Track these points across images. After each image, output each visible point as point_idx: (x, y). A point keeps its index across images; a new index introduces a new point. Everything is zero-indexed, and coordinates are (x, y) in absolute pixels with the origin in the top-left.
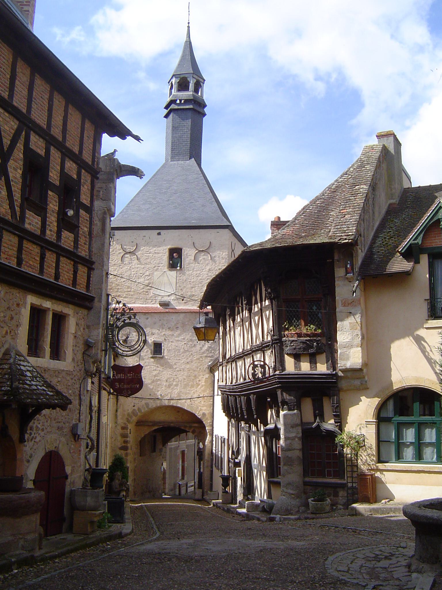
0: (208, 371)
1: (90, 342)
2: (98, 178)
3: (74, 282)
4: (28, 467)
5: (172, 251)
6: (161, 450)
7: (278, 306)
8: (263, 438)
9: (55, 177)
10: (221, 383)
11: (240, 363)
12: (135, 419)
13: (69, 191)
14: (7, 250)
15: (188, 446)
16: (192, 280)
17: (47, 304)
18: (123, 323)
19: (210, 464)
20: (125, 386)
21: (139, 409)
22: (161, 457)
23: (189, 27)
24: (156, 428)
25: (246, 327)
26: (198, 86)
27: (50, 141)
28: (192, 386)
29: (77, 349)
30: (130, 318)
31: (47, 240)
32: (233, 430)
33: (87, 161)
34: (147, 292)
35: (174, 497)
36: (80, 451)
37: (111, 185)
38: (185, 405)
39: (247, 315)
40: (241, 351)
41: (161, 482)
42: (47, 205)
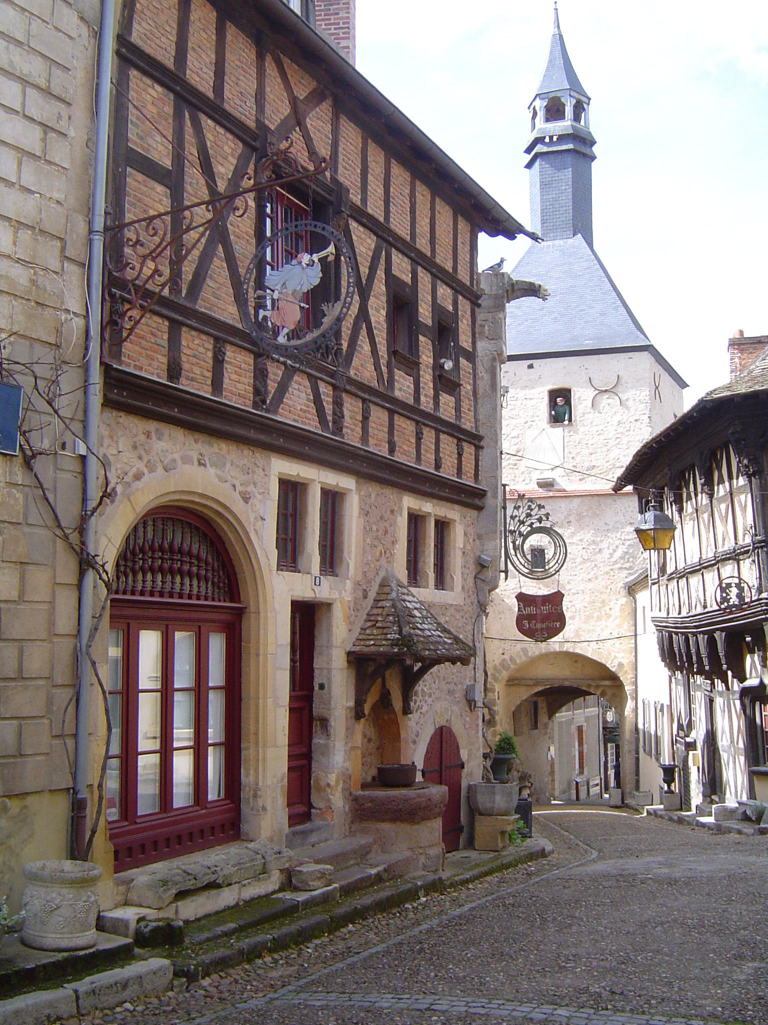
0: (624, 592)
1: (484, 560)
2: (479, 306)
3: (459, 472)
4: (415, 750)
5: (554, 395)
6: (546, 726)
7: (762, 488)
8: (738, 703)
9: (427, 313)
10: (656, 614)
11: (695, 580)
12: (505, 675)
13: (444, 331)
14: (376, 432)
15: (587, 719)
16: (590, 442)
17: (428, 507)
18: (529, 528)
19: (634, 747)
20: (539, 626)
21: (511, 658)
22: (546, 737)
23: (556, 9)
24: (540, 688)
25: (704, 521)
26: (579, 108)
27: (418, 259)
28: (599, 619)
29: (467, 571)
30: (540, 520)
31: (423, 411)
32: (680, 691)
33: (464, 280)
34: (515, 465)
35: (569, 803)
36: (477, 725)
37: (501, 316)
38: (589, 651)
39: (704, 502)
40: (696, 560)
41: (547, 779)
42: (418, 357)
